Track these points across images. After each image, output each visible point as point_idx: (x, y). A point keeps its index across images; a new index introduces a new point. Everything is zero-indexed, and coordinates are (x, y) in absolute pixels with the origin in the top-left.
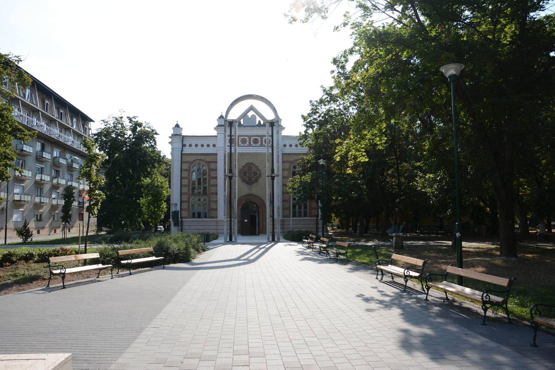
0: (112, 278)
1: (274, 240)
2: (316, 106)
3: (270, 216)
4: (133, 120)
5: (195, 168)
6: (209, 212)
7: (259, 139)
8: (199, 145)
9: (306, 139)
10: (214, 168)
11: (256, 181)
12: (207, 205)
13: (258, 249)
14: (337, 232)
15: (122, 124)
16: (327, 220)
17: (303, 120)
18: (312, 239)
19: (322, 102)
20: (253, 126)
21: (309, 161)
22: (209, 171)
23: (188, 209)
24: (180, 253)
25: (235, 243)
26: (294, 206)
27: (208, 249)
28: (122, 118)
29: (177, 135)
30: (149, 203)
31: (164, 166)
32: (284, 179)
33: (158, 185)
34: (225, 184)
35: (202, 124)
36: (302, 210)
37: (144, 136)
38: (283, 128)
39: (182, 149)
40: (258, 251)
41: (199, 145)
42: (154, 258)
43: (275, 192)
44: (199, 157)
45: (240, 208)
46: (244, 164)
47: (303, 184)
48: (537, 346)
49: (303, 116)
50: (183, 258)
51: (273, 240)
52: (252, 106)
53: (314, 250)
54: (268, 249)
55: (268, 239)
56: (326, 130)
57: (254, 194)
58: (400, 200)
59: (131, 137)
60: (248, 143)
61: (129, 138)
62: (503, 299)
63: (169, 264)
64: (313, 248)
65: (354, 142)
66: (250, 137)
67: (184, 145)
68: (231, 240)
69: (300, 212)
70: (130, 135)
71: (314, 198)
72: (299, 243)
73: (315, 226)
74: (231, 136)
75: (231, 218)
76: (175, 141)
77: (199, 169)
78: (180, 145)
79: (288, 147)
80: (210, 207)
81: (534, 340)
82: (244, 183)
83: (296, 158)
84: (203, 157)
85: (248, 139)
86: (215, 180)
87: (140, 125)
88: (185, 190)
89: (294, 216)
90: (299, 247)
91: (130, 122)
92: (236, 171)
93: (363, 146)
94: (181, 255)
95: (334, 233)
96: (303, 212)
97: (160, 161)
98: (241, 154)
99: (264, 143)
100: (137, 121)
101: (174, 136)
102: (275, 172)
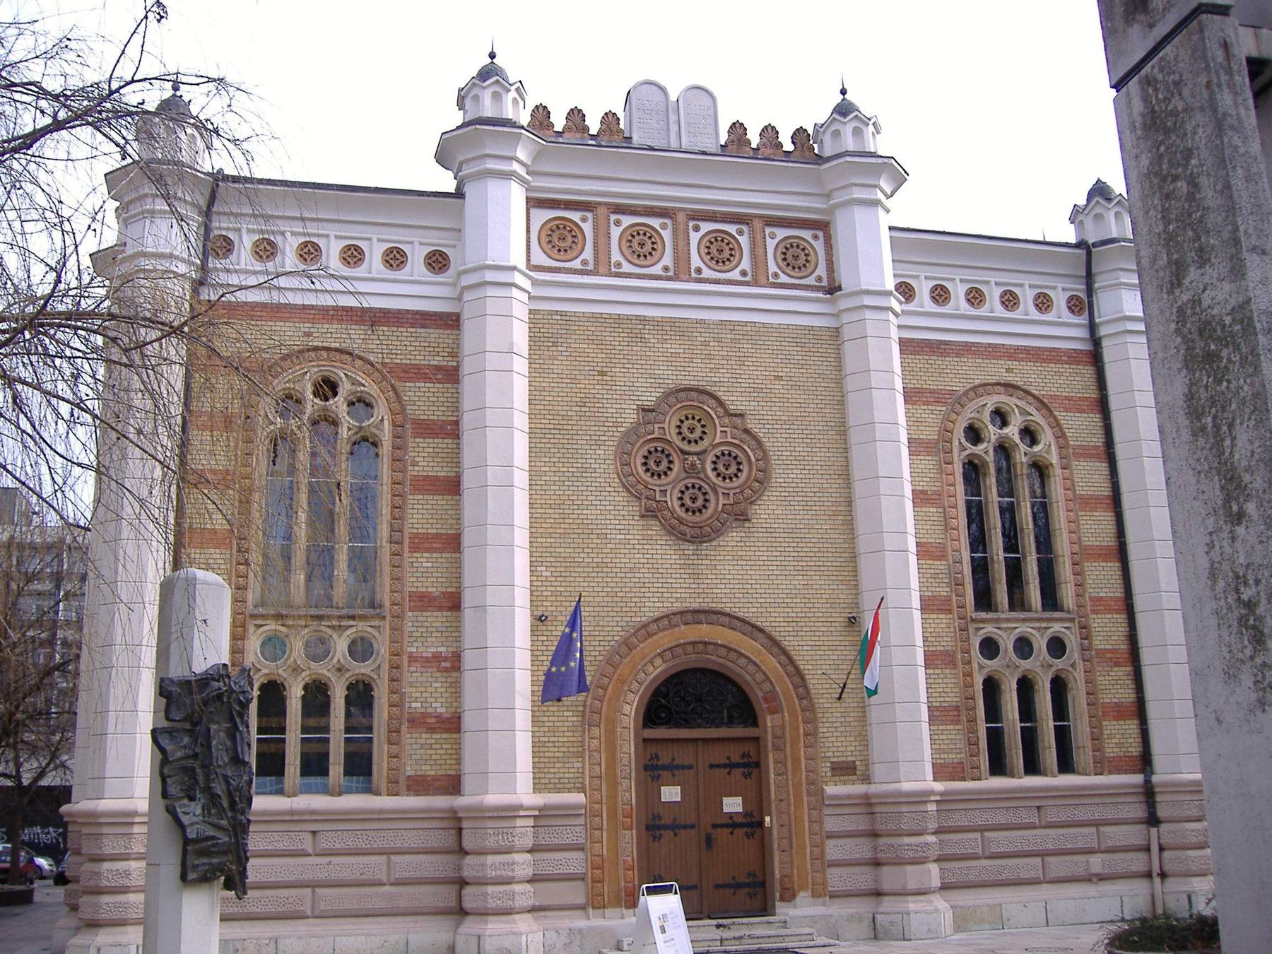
52: (1099, 180)
82: (655, 527)
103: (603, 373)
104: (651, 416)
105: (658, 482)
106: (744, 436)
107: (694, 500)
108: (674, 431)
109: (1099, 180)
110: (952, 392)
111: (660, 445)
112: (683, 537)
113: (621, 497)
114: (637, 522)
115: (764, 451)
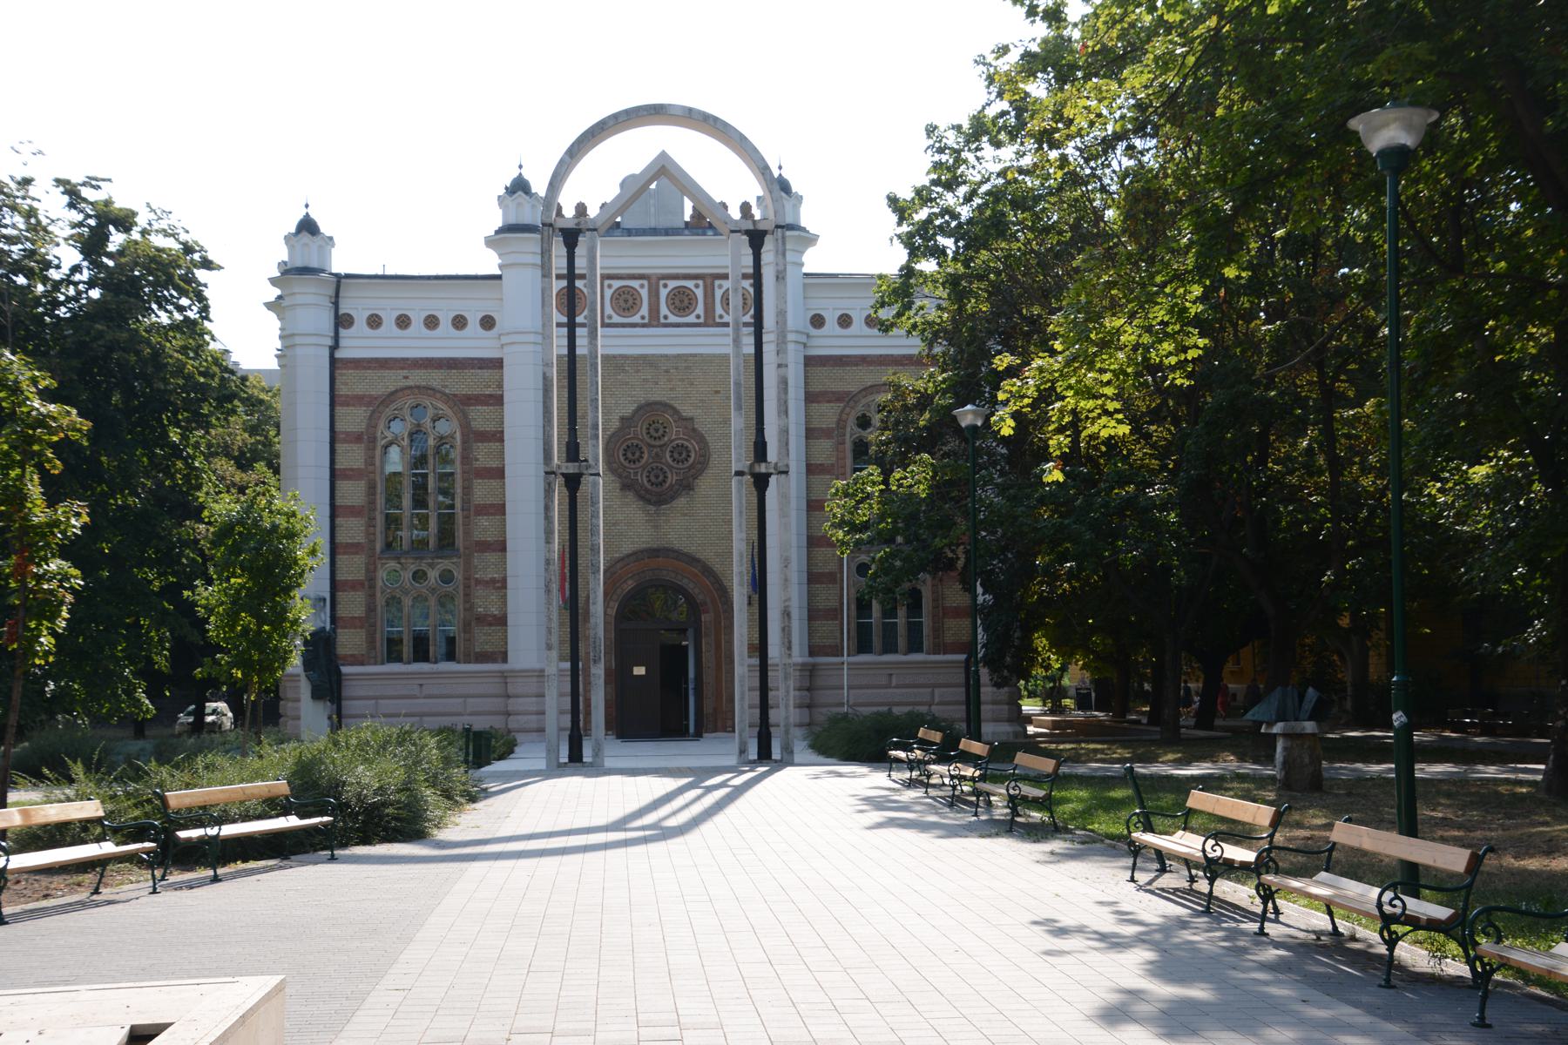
0: (154, 892)
1: (766, 753)
2: (958, 152)
3: (751, 647)
4: (86, 192)
5: (398, 428)
6: (472, 636)
7: (699, 293)
8: (417, 320)
9: (908, 306)
10: (490, 427)
11: (686, 486)
12: (459, 600)
13: (699, 791)
14: (1070, 724)
15: (31, 213)
16: (1011, 663)
17: (894, 218)
18: (924, 744)
19: (979, 129)
20: (668, 232)
21: (924, 401)
22: (464, 442)
23: (367, 621)
24: (384, 804)
25: (596, 769)
26: (863, 607)
27: (486, 794)
28: (26, 182)
29: (305, 270)
30: (237, 604)
31: (240, 418)
32: (817, 479)
33: (275, 527)
34: (548, 508)
35: (426, 224)
36: (901, 619)
37: (144, 277)
38: (810, 240)
39: (336, 338)
40: (699, 798)
41: (417, 320)
42: (293, 821)
43: (776, 539)
44: (418, 377)
45: (612, 612)
46: (629, 410)
47: (900, 508)
48: (1489, 1026)
49: (893, 201)
50: (392, 822)
51: (764, 755)
52: (663, 155)
53: (932, 792)
54: (739, 791)
55: (742, 751)
56: (1002, 267)
57: (677, 545)
58: (1340, 572)
59: (85, 275)
60: (644, 311)
61: (68, 281)
62: (1452, 911)
63: (344, 846)
64: (928, 785)
65: (1068, 363)
66: (654, 281)
67: (342, 321)
68: (576, 756)
69: (889, 632)
70: (76, 269)
71: (951, 565)
72: (877, 769)
73: (960, 693)
74: (571, 275)
75: (574, 658)
76: (299, 299)
77: (416, 433)
78: (326, 321)
79: (831, 326)
80: (470, 608)
81: (1482, 1011)
82: (631, 496)
83: (868, 377)
84: (435, 378)
85: (644, 293)
86: (494, 483)
87: (125, 221)
88: (352, 530)
89: (863, 646)
90: (873, 780)
91: (71, 205)
92: (596, 451)
93: (1106, 377)
94: (390, 810)
95: (1055, 725)
96: (902, 630)
97: (231, 397)
98: (615, 363)
99: (719, 310)
100: (108, 203)
101: (292, 274)
102: (772, 454)
109: (663, 155)
110: (848, 393)
112: (649, 502)
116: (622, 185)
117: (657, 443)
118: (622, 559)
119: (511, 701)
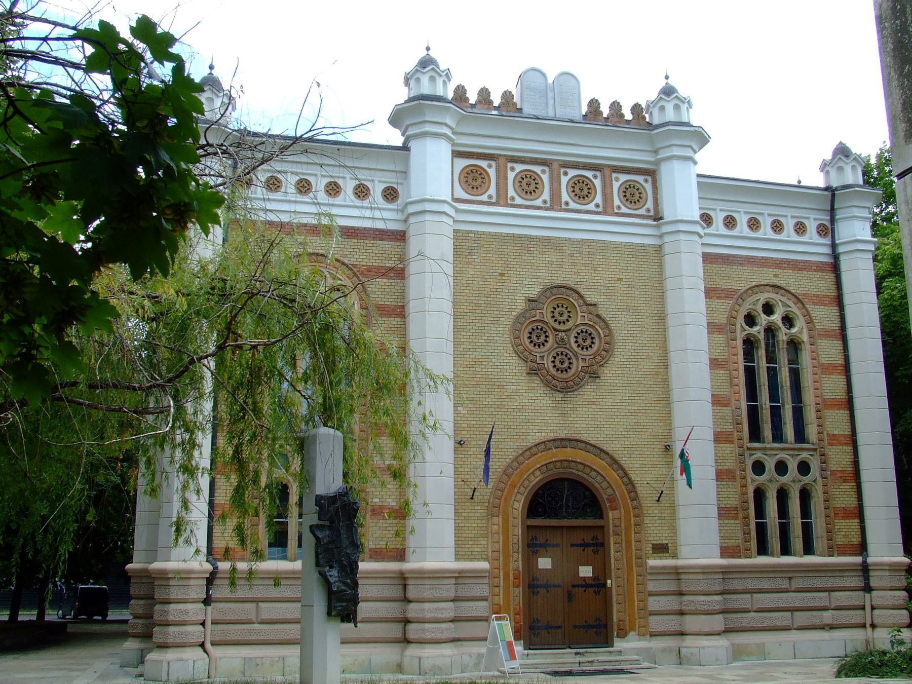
103: (502, 275)
104: (534, 305)
105: (538, 350)
106: (596, 319)
107: (562, 363)
108: (550, 315)
110: (736, 291)
111: (540, 325)
112: (555, 388)
113: (514, 360)
114: (524, 377)
115: (610, 330)
116: (530, 77)
117: (562, 327)
118: (530, 449)
119: (412, 605)
